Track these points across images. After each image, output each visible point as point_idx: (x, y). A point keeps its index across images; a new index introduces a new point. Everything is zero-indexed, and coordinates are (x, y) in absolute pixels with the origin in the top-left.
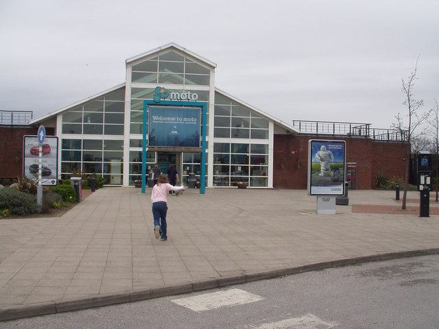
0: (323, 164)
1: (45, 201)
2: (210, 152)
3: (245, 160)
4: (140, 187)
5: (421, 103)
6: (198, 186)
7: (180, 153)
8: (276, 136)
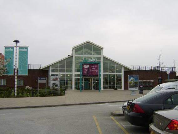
0: (132, 82)
2: (102, 77)
3: (114, 80)
5: (162, 63)
7: (89, 79)
8: (124, 71)
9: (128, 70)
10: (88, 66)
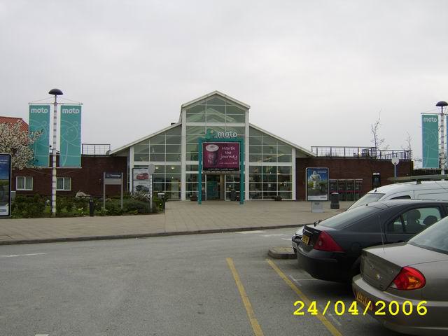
0: (314, 182)
1: (154, 207)
2: (247, 173)
3: (273, 178)
4: (196, 200)
6: (238, 199)
8: (297, 159)
10: (216, 148)
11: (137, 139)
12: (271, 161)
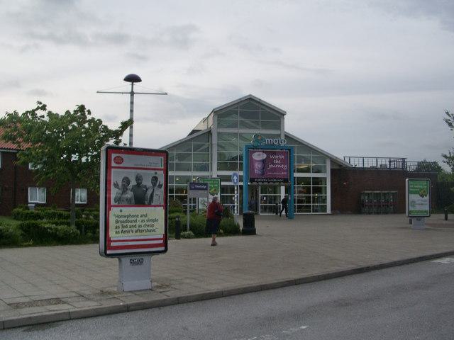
8: (333, 171)
9: (337, 167)
10: (264, 156)
11: (174, 141)
12: (184, 170)
